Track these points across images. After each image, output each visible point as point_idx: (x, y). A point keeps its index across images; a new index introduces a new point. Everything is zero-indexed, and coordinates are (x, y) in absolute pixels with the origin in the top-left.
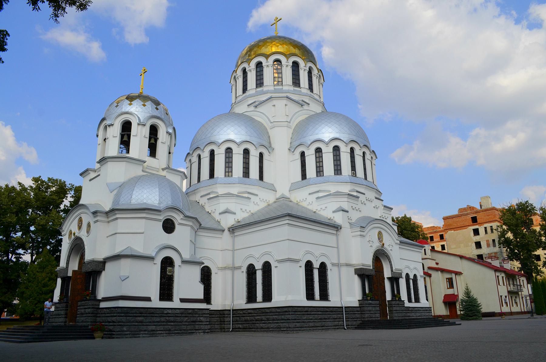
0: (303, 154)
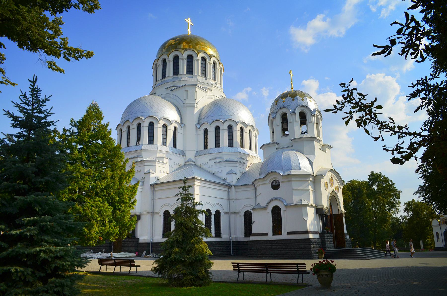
0: (206, 131)
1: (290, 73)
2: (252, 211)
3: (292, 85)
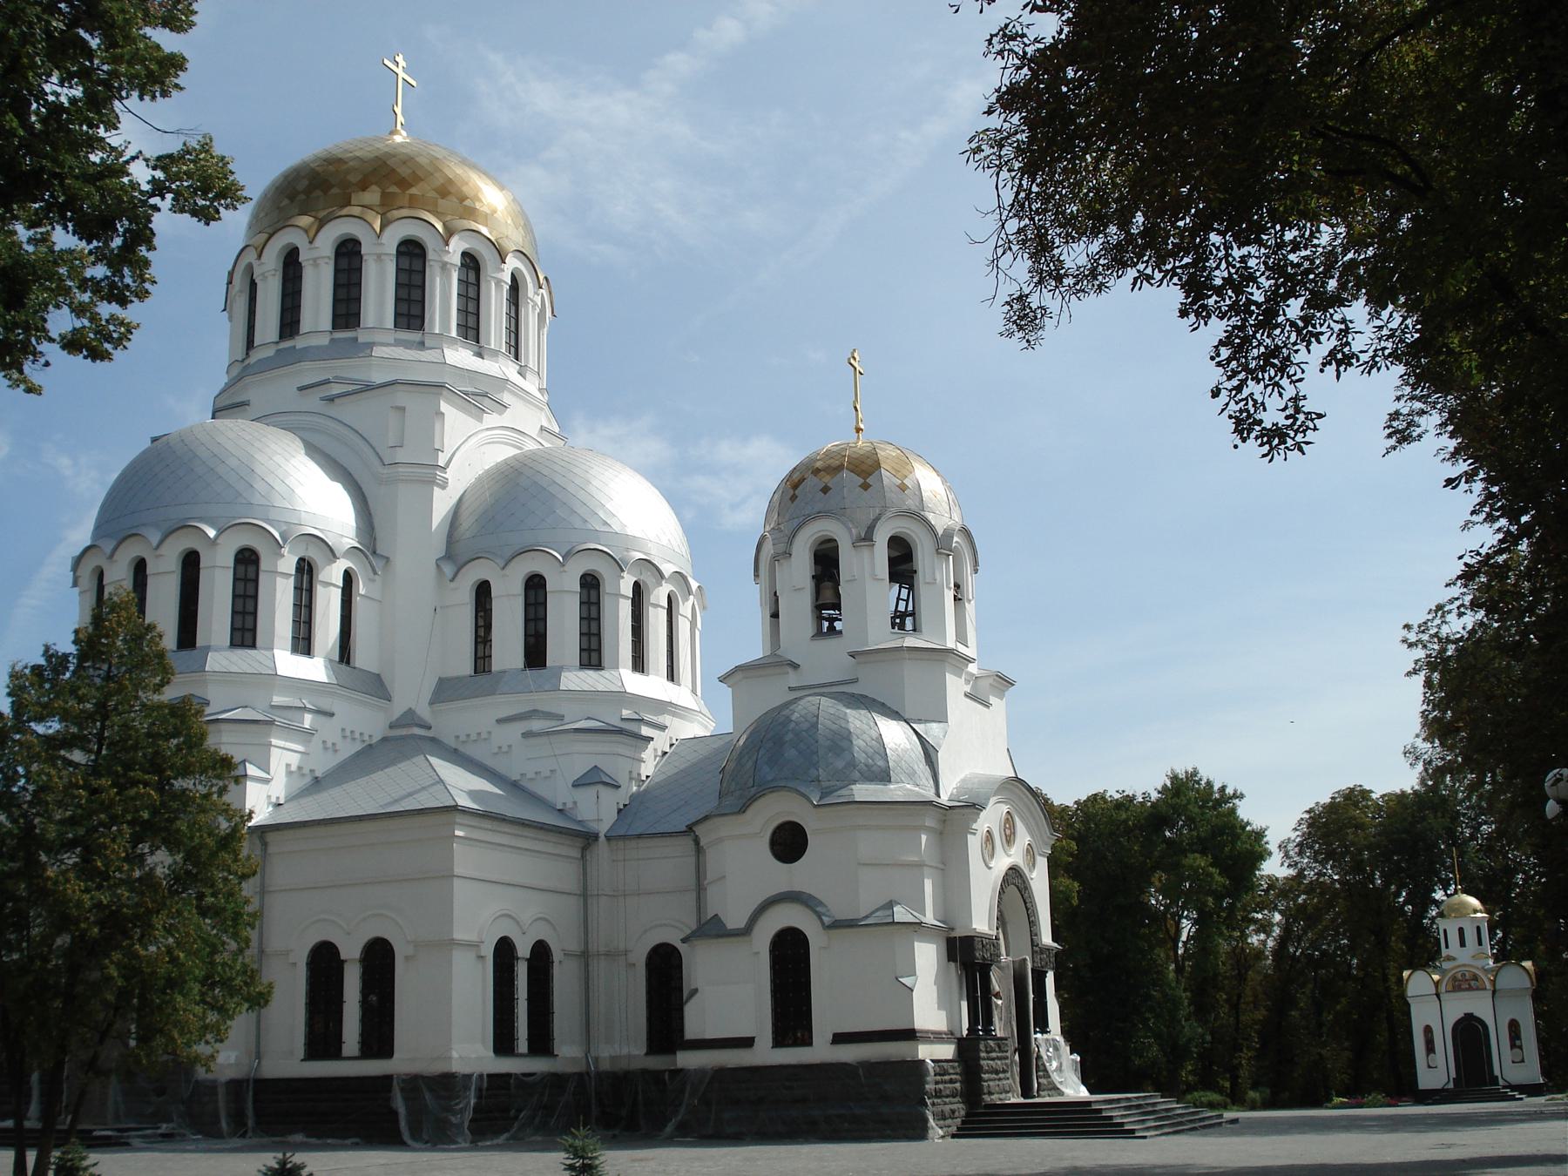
0: (483, 592)
1: (852, 361)
2: (682, 948)
3: (857, 416)
